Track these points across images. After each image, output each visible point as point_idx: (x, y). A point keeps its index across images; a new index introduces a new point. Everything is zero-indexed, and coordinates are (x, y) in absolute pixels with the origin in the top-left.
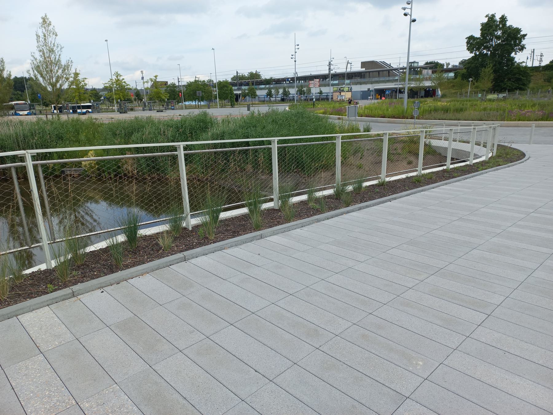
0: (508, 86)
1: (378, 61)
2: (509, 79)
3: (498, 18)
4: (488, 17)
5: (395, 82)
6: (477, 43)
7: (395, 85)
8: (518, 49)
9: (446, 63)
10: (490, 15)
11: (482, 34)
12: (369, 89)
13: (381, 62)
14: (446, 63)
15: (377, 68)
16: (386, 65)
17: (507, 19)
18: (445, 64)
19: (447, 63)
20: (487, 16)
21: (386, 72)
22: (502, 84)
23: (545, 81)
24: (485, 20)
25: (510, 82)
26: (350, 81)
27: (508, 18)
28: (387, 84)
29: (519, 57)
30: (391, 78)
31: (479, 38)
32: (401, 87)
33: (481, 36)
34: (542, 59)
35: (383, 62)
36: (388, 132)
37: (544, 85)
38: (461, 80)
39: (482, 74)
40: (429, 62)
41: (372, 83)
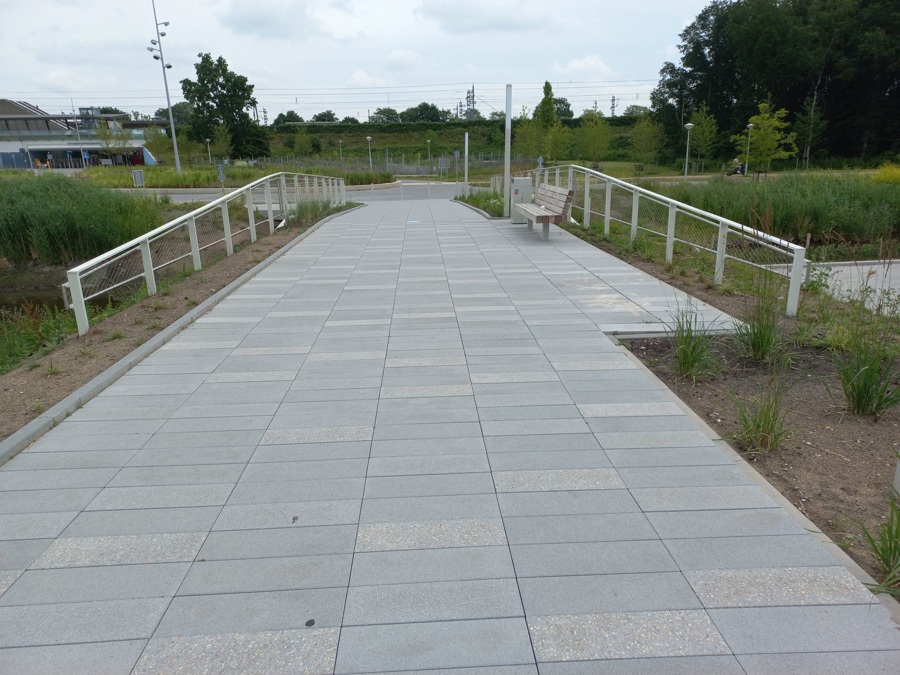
0: (249, 150)
1: (15, 100)
2: (248, 142)
3: (214, 59)
4: (201, 57)
5: (67, 139)
6: (197, 91)
7: (69, 144)
8: (249, 103)
9: (133, 112)
10: (204, 53)
11: (201, 79)
12: (22, 150)
13: (20, 102)
14: (133, 112)
15: (15, 114)
16: (32, 109)
17: (226, 62)
18: (132, 114)
19: (134, 112)
20: (200, 55)
21: (41, 121)
22: (241, 148)
23: (285, 146)
24: (199, 61)
25: (249, 146)
26: (145, 132)
27: (228, 62)
28: (38, 142)
29: (251, 113)
30: (54, 133)
31: (195, 84)
32: (99, 148)
33: (198, 80)
34: (266, 116)
35: (25, 102)
36: (521, 178)
37: (285, 150)
38: (188, 140)
39: (216, 133)
40: (340, 116)
41: (21, 139)
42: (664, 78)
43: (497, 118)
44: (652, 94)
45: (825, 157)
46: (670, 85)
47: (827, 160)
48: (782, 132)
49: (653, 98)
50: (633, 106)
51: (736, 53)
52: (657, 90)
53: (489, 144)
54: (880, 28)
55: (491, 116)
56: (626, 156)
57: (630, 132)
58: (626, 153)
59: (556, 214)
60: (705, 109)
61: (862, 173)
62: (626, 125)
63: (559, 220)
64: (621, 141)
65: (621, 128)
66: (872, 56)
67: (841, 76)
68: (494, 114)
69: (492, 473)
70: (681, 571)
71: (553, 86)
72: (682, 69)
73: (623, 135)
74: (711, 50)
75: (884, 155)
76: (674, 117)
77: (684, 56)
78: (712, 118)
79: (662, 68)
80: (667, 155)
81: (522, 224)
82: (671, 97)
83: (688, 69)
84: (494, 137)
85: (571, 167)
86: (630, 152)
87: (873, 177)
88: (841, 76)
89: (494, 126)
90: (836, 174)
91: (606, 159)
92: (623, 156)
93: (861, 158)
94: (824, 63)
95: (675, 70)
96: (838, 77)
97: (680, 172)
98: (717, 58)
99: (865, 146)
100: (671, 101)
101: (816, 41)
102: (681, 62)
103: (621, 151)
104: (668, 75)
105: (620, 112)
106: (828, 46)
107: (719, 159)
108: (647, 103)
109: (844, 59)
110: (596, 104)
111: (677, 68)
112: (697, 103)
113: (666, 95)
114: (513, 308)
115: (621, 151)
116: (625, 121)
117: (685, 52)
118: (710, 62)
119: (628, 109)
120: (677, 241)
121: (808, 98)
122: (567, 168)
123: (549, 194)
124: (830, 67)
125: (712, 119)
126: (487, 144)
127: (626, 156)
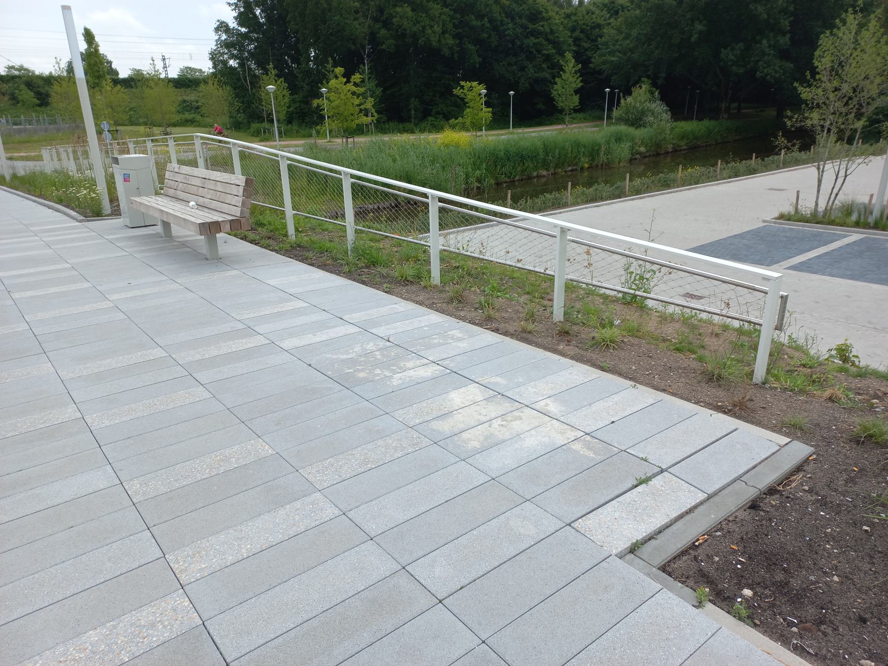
42: (220, 38)
43: (17, 73)
44: (210, 54)
45: (384, 122)
46: (227, 45)
47: (387, 126)
48: (361, 97)
49: (212, 59)
50: (186, 68)
51: (289, 16)
52: (215, 50)
53: (14, 104)
54: (406, 5)
55: (6, 70)
56: (195, 121)
57: (192, 95)
58: (193, 118)
59: (231, 218)
60: (273, 72)
61: (431, 137)
62: (186, 88)
63: (236, 228)
64: (185, 105)
65: (180, 90)
66: (405, 30)
67: (384, 47)
68: (10, 68)
69: (205, 624)
70: (344, 514)
71: (94, 31)
72: (237, 29)
73: (186, 98)
74: (262, 11)
75: (428, 121)
76: (239, 79)
77: (236, 15)
78: (282, 81)
79: (216, 26)
80: (240, 120)
81: (145, 226)
82: (232, 59)
83: (243, 30)
84: (19, 97)
85: (198, 136)
86: (198, 118)
87: (439, 141)
88: (384, 47)
89: (15, 83)
90: (412, 137)
91: (174, 125)
92: (190, 121)
93: (412, 124)
94: (368, 33)
95: (229, 29)
96: (382, 47)
97: (259, 138)
98: (268, 18)
99: (413, 112)
100: (232, 63)
101: (357, 12)
102: (234, 21)
103: (188, 116)
104: (224, 34)
105: (173, 74)
106: (367, 18)
107: (294, 124)
108: (206, 66)
109: (383, 32)
110: (153, 61)
111: (232, 27)
112: (262, 65)
113: (226, 56)
114: (158, 353)
115: (188, 116)
116: (184, 83)
117: (237, 11)
118: (264, 24)
119: (182, 70)
120: (296, 214)
121: (361, 66)
122: (192, 138)
123: (197, 182)
124: (373, 38)
125: (283, 83)
126: (11, 104)
127: (195, 121)
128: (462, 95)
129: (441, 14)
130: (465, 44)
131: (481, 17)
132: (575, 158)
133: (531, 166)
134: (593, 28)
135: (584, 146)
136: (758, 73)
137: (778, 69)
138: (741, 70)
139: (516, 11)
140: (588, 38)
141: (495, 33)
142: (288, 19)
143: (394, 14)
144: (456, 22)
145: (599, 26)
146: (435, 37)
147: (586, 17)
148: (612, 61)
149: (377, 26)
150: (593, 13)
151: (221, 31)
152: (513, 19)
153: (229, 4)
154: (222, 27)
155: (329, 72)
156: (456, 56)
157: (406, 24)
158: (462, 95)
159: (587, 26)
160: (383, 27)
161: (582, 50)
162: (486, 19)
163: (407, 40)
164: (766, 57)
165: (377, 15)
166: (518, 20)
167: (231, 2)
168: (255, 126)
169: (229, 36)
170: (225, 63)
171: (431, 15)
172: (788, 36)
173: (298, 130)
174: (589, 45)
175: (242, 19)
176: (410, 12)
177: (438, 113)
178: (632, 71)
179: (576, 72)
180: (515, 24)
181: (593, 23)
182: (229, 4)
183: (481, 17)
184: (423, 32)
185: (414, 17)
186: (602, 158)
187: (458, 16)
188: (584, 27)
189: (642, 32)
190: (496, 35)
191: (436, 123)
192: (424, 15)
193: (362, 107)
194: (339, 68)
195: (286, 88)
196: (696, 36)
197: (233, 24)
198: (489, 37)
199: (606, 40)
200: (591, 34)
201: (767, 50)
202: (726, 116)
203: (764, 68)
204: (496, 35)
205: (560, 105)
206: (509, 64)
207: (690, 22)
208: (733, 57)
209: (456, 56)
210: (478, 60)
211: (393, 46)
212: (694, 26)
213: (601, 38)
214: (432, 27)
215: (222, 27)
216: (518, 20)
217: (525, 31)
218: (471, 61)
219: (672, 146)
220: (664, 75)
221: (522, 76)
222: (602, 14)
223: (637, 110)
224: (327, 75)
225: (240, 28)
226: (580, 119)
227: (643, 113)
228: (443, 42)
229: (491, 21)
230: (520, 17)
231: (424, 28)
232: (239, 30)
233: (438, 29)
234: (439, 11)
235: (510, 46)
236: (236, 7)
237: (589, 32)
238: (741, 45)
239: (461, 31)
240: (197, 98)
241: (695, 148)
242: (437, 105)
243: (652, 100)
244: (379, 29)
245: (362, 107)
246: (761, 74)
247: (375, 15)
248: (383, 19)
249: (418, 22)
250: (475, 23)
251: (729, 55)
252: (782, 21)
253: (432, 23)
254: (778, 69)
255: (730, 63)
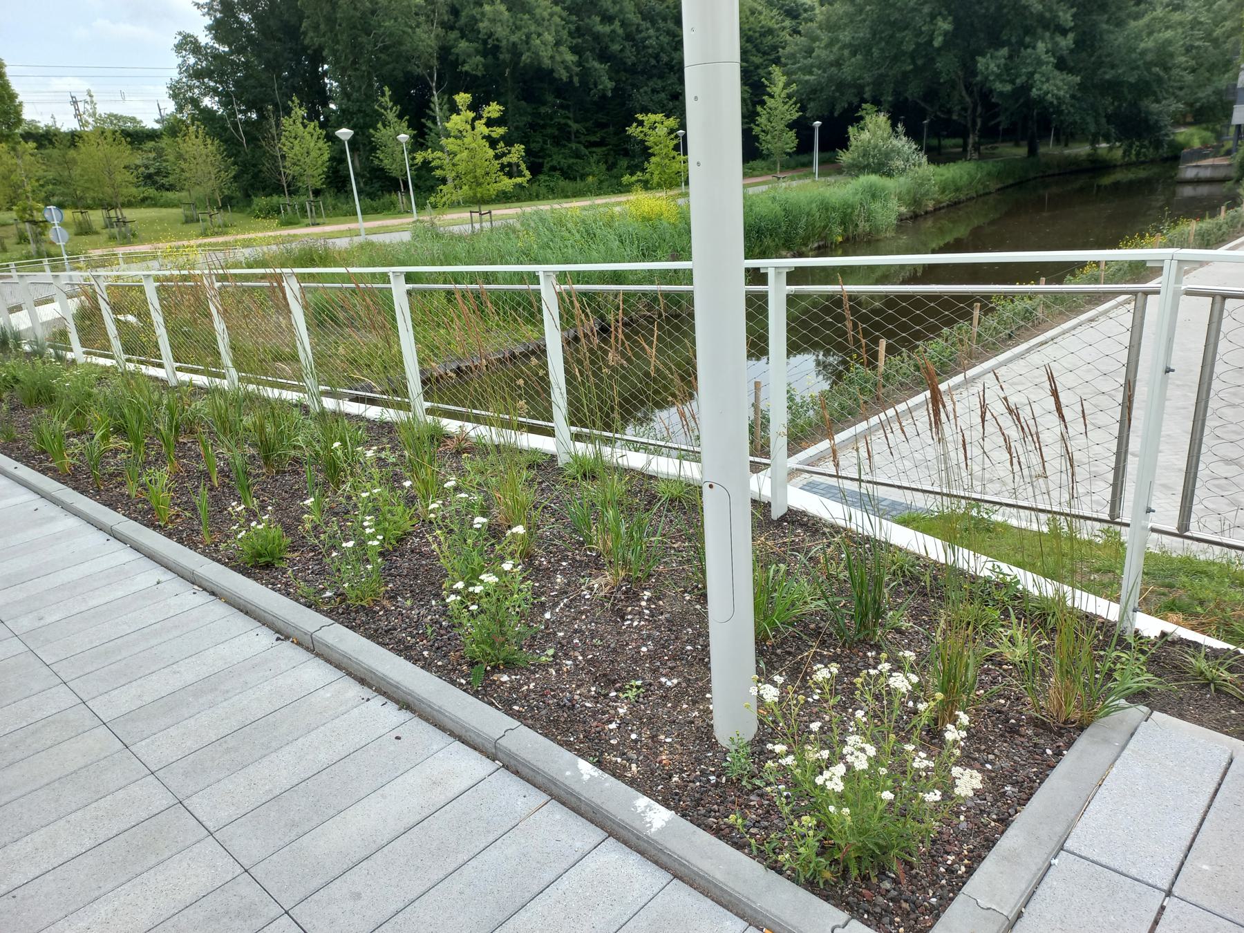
44: (170, 88)
49: (174, 96)
52: (177, 82)
76: (226, 129)
79: (176, 42)
88: (466, 68)
95: (201, 47)
109: (463, 44)
110: (91, 96)
111: (203, 44)
125: (317, 129)
128: (642, 135)
129: (551, 15)
130: (587, 62)
131: (607, 19)
132: (825, 227)
133: (772, 244)
134: (763, 35)
135: (834, 209)
136: (1034, 90)
137: (1060, 84)
138: (1008, 88)
139: (657, 11)
140: (758, 51)
141: (631, 43)
142: (302, 29)
143: (478, 17)
144: (573, 27)
145: (770, 31)
146: (546, 51)
147: (752, 19)
148: (807, 82)
149: (454, 35)
150: (760, 13)
151: (185, 50)
152: (653, 22)
153: (197, 4)
154: (187, 44)
155: (386, 110)
156: (576, 79)
157: (501, 31)
158: (642, 135)
159: (755, 32)
160: (462, 38)
161: (752, 68)
162: (617, 23)
163: (501, 57)
164: (1044, 67)
165: (449, 20)
166: (661, 24)
167: (201, 3)
168: (261, 201)
169: (199, 59)
170: (195, 102)
171: (538, 16)
172: (1071, 36)
173: (336, 205)
174: (761, 60)
175: (219, 29)
176: (506, 13)
177: (553, 169)
178: (837, 94)
179: (789, 97)
180: (658, 30)
181: (762, 27)
182: (197, 4)
183: (607, 19)
184: (527, 43)
185: (511, 20)
186: (863, 226)
187: (574, 18)
188: (751, 33)
189: (856, 35)
190: (632, 47)
191: (552, 184)
192: (527, 16)
193: (505, 160)
194: (462, 94)
195: (322, 136)
196: (940, 39)
197: (205, 39)
198: (622, 51)
199: (792, 51)
200: (761, 43)
201: (1044, 57)
202: (976, 156)
203: (1043, 83)
204: (632, 47)
205: (764, 147)
206: (654, 91)
207: (928, 19)
208: (995, 69)
209: (576, 79)
210: (610, 85)
211: (480, 67)
212: (936, 24)
213: (784, 48)
214: (539, 35)
215: (187, 44)
216: (661, 24)
217: (673, 40)
218: (600, 87)
219: (933, 202)
220: (890, 99)
221: (675, 108)
222: (772, 14)
223: (880, 150)
224: (383, 114)
225: (217, 46)
226: (762, 169)
227: (888, 155)
228: (558, 58)
229: (623, 24)
230: (665, 20)
231: (528, 36)
232: (216, 49)
233: (549, 38)
234: (549, 10)
235: (653, 62)
236: (209, 10)
237: (759, 41)
238: (1004, 51)
239: (580, 41)
240: (145, 162)
241: (955, 203)
242: (551, 156)
243: (896, 134)
244: (456, 40)
245: (505, 160)
246: (1039, 93)
247: (446, 18)
248: (454, 21)
249: (518, 28)
250: (602, 29)
251: (989, 64)
252: (1061, 14)
253: (540, 30)
254: (1060, 84)
255: (991, 78)
